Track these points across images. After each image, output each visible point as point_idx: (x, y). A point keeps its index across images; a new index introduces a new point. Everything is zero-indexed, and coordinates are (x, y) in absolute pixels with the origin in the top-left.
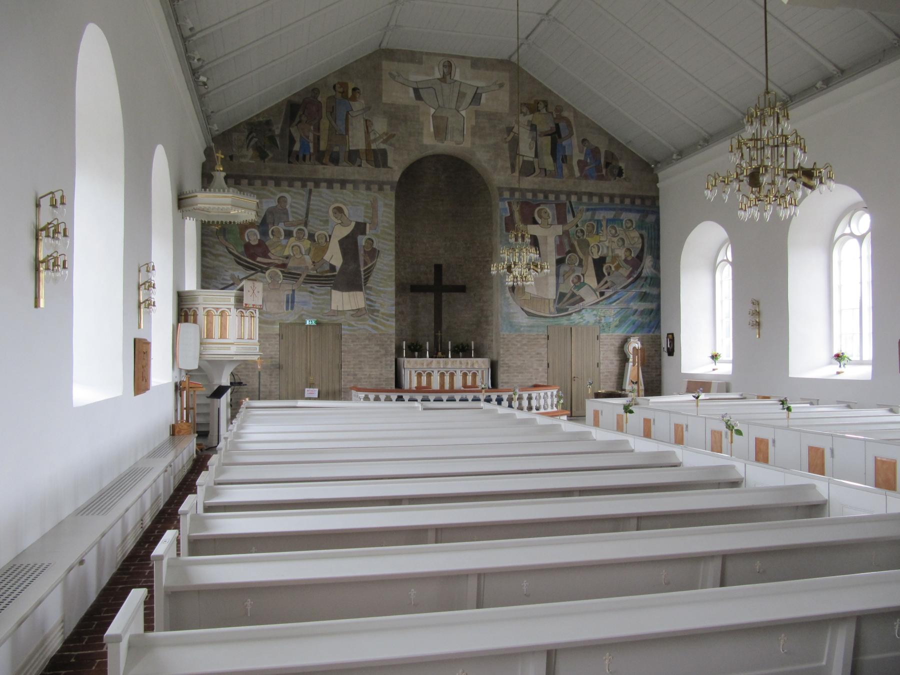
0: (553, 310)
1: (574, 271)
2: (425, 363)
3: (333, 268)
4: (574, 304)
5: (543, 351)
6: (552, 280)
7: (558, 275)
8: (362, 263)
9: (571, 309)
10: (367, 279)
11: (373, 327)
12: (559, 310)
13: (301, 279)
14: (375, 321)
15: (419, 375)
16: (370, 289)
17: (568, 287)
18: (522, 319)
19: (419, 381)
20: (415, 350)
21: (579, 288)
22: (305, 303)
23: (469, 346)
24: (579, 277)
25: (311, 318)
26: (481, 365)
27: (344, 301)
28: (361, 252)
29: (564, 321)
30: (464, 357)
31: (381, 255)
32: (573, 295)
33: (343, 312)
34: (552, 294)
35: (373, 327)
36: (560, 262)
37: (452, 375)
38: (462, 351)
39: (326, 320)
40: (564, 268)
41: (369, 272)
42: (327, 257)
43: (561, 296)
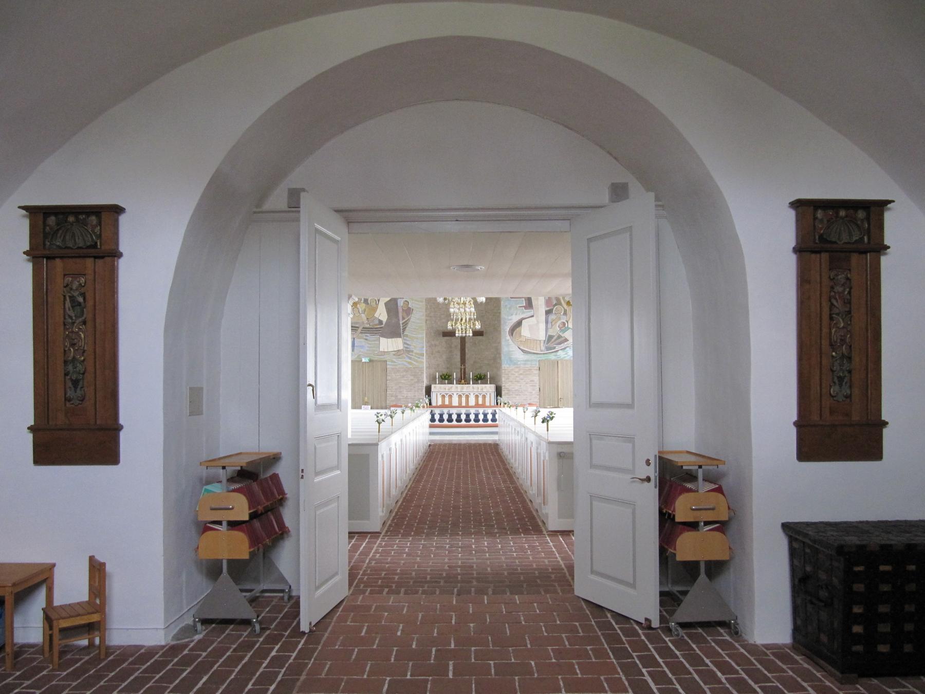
0: (543, 348)
1: (560, 319)
2: (455, 389)
3: (381, 322)
4: (560, 343)
5: (536, 379)
6: (543, 326)
7: (547, 322)
8: (401, 318)
9: (558, 348)
10: (404, 329)
11: (409, 363)
12: (548, 349)
13: (359, 330)
14: (410, 358)
15: (443, 397)
16: (407, 336)
17: (555, 331)
18: (519, 355)
19: (443, 401)
20: (446, 378)
21: (564, 331)
22: (362, 347)
23: (485, 376)
24: (564, 324)
25: (365, 357)
26: (490, 388)
27: (388, 345)
28: (400, 310)
29: (552, 357)
30: (482, 383)
31: (414, 312)
32: (559, 337)
33: (388, 352)
34: (542, 336)
35: (409, 363)
36: (548, 312)
37: (467, 397)
38: (480, 379)
39: (376, 358)
40: (552, 317)
41: (405, 324)
42: (376, 315)
43: (550, 338)
